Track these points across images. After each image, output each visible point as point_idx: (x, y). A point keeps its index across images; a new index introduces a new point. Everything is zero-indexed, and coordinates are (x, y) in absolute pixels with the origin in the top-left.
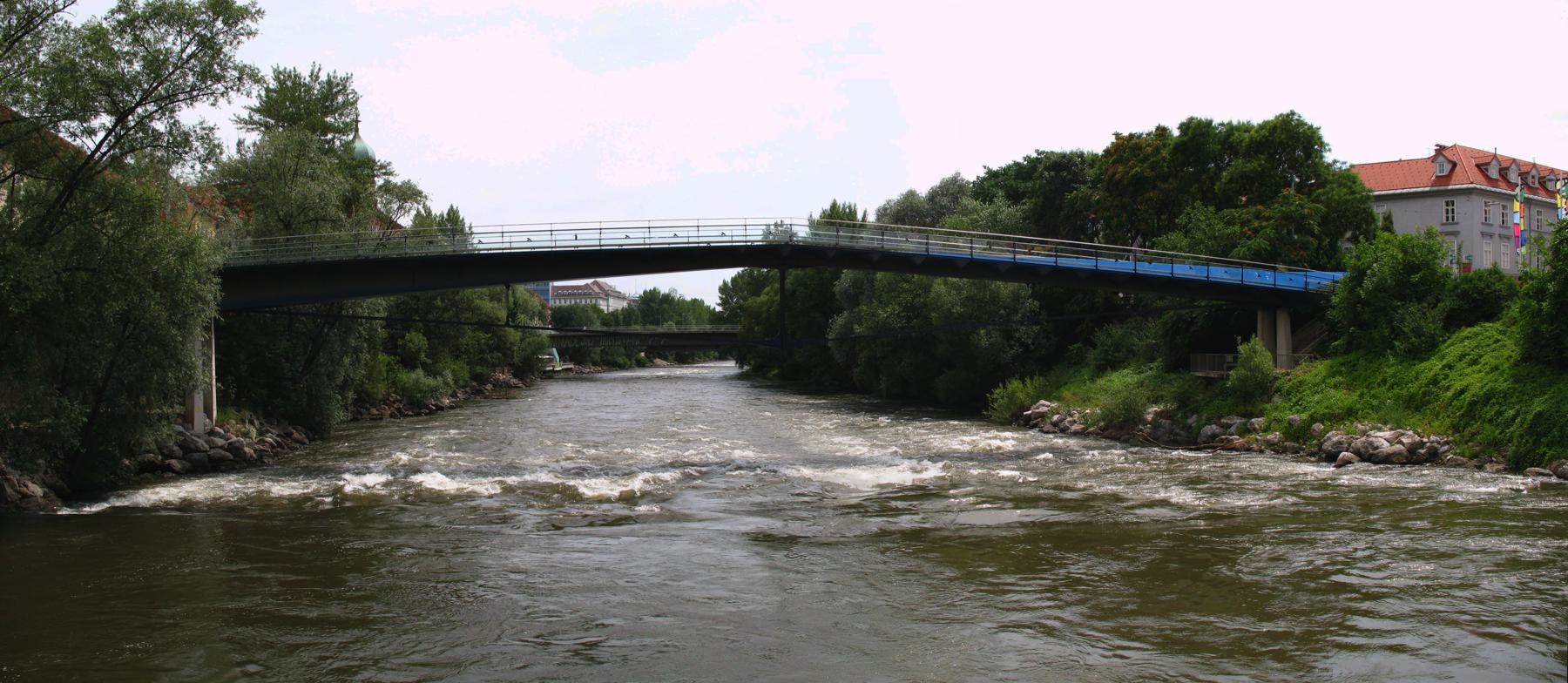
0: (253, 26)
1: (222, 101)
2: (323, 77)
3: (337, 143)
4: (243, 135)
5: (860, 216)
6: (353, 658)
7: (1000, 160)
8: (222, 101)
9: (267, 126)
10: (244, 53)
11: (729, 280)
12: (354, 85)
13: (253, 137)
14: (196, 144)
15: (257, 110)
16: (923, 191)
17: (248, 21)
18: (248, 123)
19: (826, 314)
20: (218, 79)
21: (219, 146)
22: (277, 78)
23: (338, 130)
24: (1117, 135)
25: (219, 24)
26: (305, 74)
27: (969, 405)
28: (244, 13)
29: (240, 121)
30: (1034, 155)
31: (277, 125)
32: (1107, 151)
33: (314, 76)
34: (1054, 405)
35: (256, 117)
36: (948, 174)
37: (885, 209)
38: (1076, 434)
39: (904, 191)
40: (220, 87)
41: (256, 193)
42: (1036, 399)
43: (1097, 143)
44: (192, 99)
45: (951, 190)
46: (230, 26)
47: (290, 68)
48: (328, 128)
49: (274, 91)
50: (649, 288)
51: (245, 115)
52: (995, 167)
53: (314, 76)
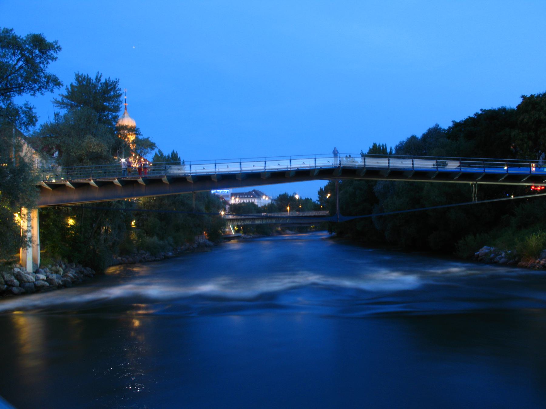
0: (55, 55)
1: (38, 94)
2: (103, 80)
3: (110, 117)
4: (57, 110)
5: (388, 151)
6: (533, 267)
7: (461, 117)
8: (38, 94)
9: (72, 106)
10: (51, 69)
11: (323, 187)
12: (120, 86)
13: (63, 112)
14: (22, 116)
15: (66, 97)
16: (419, 135)
17: (52, 52)
18: (61, 104)
19: (369, 208)
20: (35, 81)
21: (35, 117)
22: (77, 79)
23: (110, 110)
24: (524, 97)
25: (37, 52)
26: (93, 77)
27: (448, 252)
28: (50, 47)
29: (57, 102)
30: (480, 112)
31: (77, 106)
32: (519, 107)
33: (98, 79)
34: (492, 249)
35: (66, 101)
36: (432, 125)
37: (400, 147)
38: (504, 265)
39: (409, 136)
40: (36, 86)
41: (64, 143)
42: (481, 247)
43: (513, 102)
44: (20, 92)
45: (434, 133)
46: (43, 53)
47: (85, 73)
48: (104, 109)
49: (76, 87)
50: (282, 193)
51: (59, 99)
52: (458, 120)
53: (98, 79)
